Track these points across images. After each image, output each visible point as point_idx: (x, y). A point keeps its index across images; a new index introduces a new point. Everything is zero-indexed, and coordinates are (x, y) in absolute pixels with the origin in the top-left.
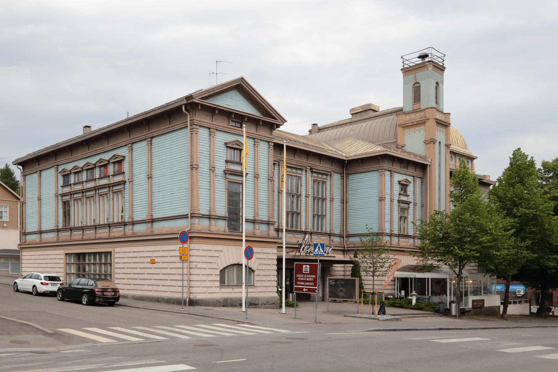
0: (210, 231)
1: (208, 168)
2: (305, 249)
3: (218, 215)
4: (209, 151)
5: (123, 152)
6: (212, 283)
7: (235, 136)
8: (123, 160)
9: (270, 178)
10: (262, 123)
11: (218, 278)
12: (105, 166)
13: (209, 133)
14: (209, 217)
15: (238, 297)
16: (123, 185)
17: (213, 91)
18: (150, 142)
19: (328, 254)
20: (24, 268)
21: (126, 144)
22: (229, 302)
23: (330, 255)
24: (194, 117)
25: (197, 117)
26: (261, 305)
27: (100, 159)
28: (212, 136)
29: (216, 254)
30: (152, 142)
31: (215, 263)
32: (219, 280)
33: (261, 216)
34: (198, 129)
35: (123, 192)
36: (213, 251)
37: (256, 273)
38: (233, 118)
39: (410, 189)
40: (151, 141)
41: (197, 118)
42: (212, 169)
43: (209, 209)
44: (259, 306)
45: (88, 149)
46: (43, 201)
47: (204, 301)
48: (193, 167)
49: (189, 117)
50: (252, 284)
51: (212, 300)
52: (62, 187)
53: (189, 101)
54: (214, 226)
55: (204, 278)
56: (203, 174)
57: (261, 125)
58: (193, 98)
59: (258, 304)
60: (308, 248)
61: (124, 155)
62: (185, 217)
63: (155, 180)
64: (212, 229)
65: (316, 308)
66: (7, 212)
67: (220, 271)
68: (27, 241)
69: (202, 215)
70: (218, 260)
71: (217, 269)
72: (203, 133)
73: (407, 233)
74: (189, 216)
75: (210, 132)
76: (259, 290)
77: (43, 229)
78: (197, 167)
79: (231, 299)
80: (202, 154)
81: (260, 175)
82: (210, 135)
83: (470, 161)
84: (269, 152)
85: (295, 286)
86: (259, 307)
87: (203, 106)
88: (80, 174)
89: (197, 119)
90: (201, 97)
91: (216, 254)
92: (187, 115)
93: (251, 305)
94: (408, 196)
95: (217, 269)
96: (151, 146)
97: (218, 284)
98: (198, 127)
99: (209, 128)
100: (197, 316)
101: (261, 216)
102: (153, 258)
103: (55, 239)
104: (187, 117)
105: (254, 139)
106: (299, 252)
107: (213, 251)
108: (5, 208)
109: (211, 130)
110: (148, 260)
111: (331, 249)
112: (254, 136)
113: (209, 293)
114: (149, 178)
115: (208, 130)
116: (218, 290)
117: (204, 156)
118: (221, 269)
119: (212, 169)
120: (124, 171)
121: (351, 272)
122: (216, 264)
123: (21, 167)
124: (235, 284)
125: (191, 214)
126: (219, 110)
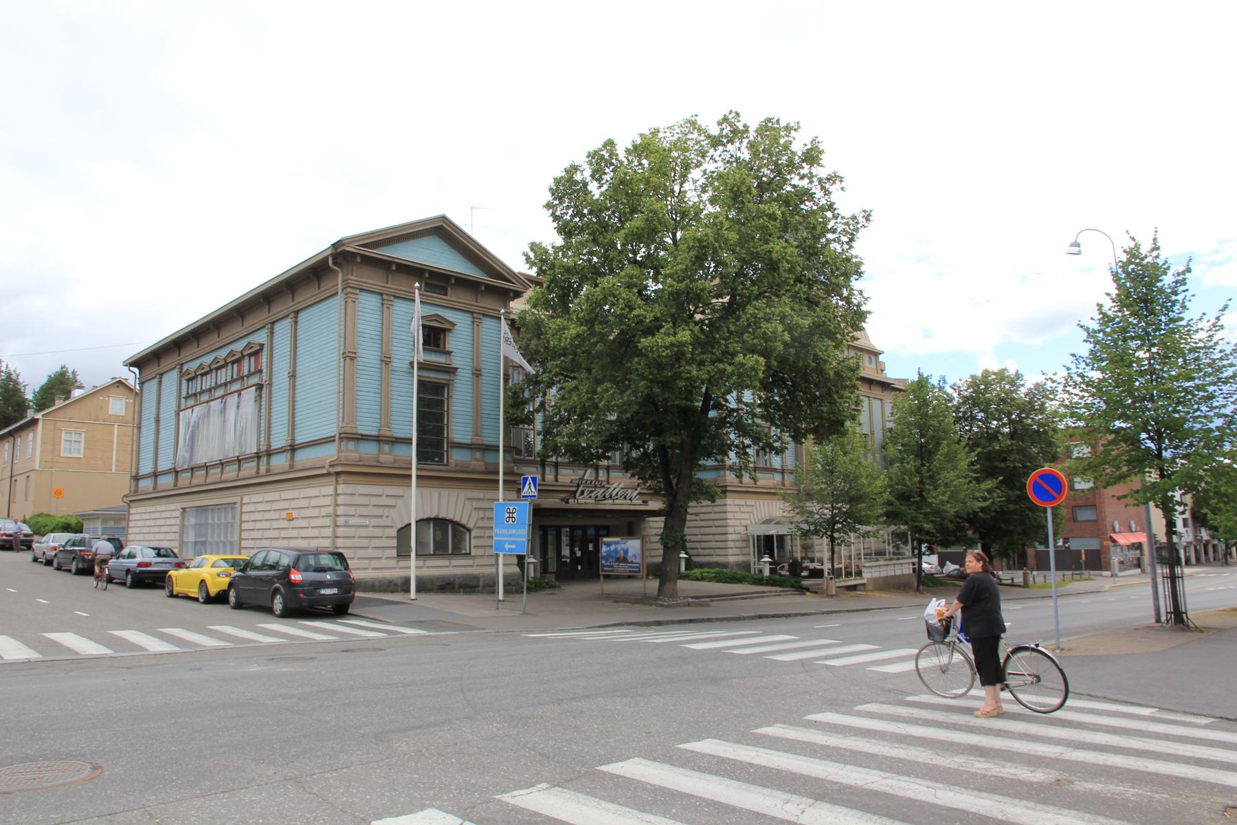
0: (378, 462)
1: (378, 358)
2: (585, 494)
3: (396, 435)
4: (380, 330)
5: (261, 337)
6: (381, 551)
7: (433, 308)
9: (384, 359)
10: (397, 268)
11: (394, 543)
12: (238, 361)
13: (381, 301)
14: (378, 439)
17: (385, 234)
19: (630, 499)
20: (132, 535)
23: (634, 502)
25: (354, 273)
26: (484, 587)
28: (385, 306)
29: (391, 502)
31: (387, 517)
32: (396, 545)
33: (485, 439)
34: (357, 294)
36: (384, 497)
37: (473, 534)
38: (426, 278)
39: (452, 342)
41: (392, 284)
42: (386, 361)
43: (378, 425)
44: (480, 589)
46: (162, 423)
48: (350, 357)
49: (340, 275)
50: (468, 551)
51: (380, 582)
52: (186, 398)
53: (339, 250)
54: (387, 454)
55: (365, 542)
57: (395, 271)
58: (343, 245)
59: (477, 586)
60: (591, 492)
62: (328, 440)
63: (299, 381)
64: (381, 460)
65: (645, 588)
66: (79, 442)
67: (398, 531)
68: (139, 489)
69: (362, 435)
70: (392, 512)
71: (391, 527)
72: (369, 303)
73: (771, 464)
74: (337, 438)
75: (383, 300)
76: (478, 561)
78: (354, 355)
81: (483, 370)
82: (383, 304)
83: (873, 358)
84: (473, 329)
86: (479, 592)
87: (364, 258)
89: (355, 278)
90: (362, 243)
91: (391, 502)
92: (338, 272)
94: (449, 353)
95: (391, 527)
97: (394, 553)
98: (357, 291)
99: (381, 294)
101: (485, 439)
102: (290, 511)
103: (171, 486)
104: (338, 276)
105: (472, 313)
106: (575, 498)
107: (384, 497)
108: (68, 435)
109: (385, 297)
110: (284, 515)
111: (637, 492)
112: (472, 309)
113: (374, 569)
115: (379, 297)
116: (393, 563)
118: (399, 527)
119: (386, 361)
121: (662, 530)
122: (389, 519)
123: (136, 370)
124: (432, 552)
125: (340, 434)
126: (398, 265)
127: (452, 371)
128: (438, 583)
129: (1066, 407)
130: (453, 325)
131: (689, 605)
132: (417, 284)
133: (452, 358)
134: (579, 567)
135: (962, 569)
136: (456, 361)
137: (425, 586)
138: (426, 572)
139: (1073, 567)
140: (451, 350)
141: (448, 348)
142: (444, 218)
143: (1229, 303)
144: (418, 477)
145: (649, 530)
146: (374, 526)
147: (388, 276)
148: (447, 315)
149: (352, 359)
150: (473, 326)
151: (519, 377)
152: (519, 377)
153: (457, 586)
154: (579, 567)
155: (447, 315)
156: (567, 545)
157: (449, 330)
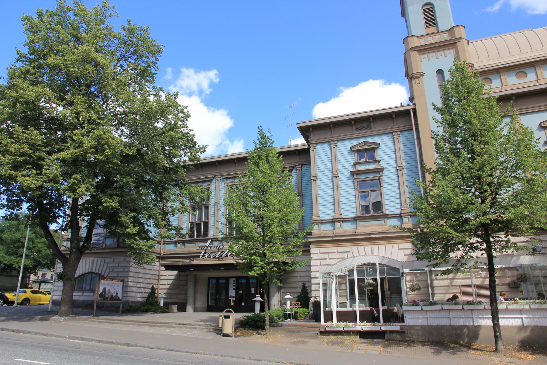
9: (398, 168)
39: (379, 154)
41: (374, 128)
54: (339, 228)
78: (337, 175)
94: (379, 161)
109: (394, 134)
127: (382, 170)
130: (379, 144)
136: (382, 165)
139: (465, 331)
140: (379, 159)
141: (377, 158)
143: (2, 78)
146: (169, 275)
149: (336, 177)
150: (331, 149)
154: (243, 304)
156: (234, 289)
157: (377, 148)
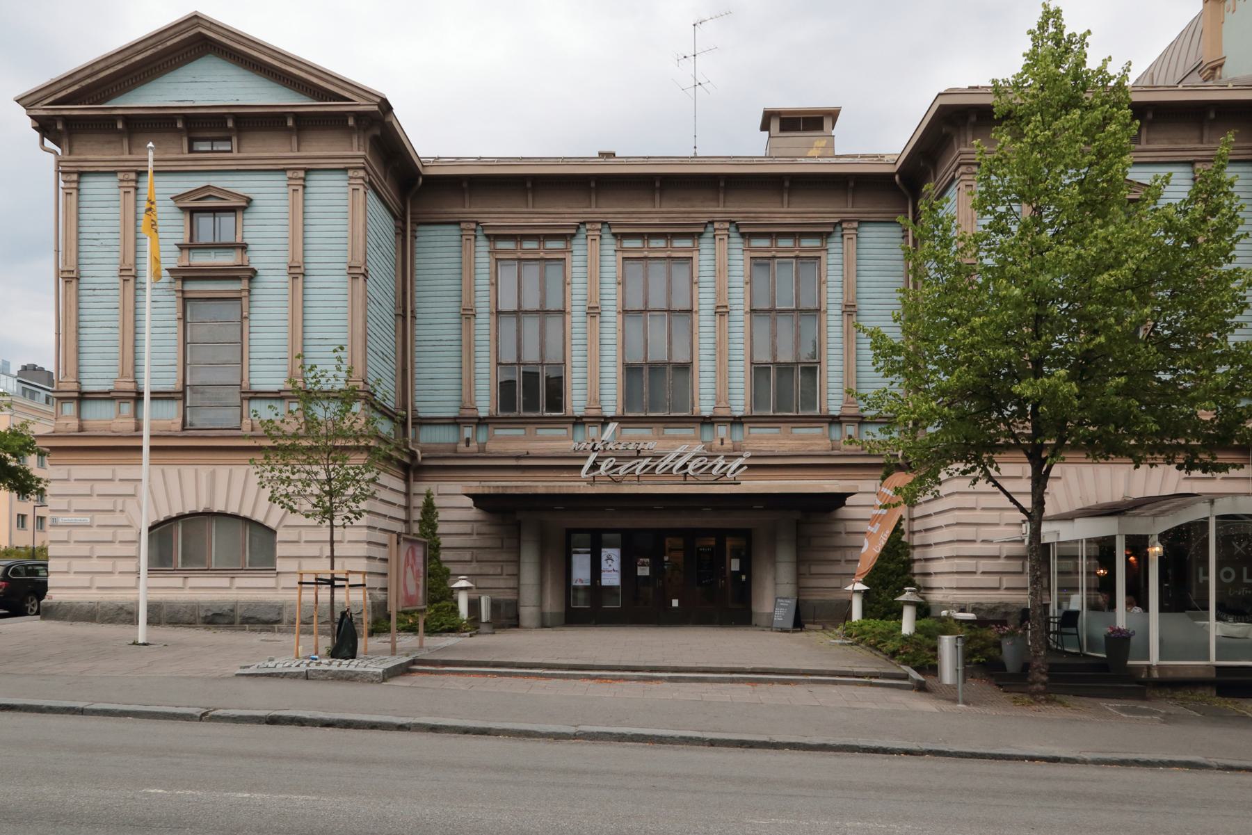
8: (243, 209)
15: (201, 599)
16: (245, 282)
18: (74, 185)
21: (282, 167)
22: (165, 611)
24: (963, 145)
27: (209, 186)
30: (308, 184)
31: (121, 511)
35: (245, 301)
36: (117, 482)
40: (78, 182)
44: (283, 626)
45: (299, 145)
47: (72, 607)
51: (103, 607)
56: (97, 292)
61: (251, 196)
77: (88, 386)
79: (171, 605)
80: (95, 242)
85: (1154, 659)
86: (280, 631)
88: (239, 215)
93: (247, 623)
96: (79, 195)
100: (787, 756)
107: (117, 482)
114: (294, 277)
117: (102, 245)
120: (246, 241)
128: (202, 614)
129: (1087, 77)
131: (372, 681)
132: (150, 145)
133: (249, 254)
134: (675, 603)
135: (364, 628)
137: (160, 615)
138: (159, 596)
142: (195, 19)
144: (153, 449)
145: (843, 535)
147: (352, 140)
148: (237, 184)
151: (852, 284)
152: (852, 284)
153: (238, 620)
155: (237, 184)
